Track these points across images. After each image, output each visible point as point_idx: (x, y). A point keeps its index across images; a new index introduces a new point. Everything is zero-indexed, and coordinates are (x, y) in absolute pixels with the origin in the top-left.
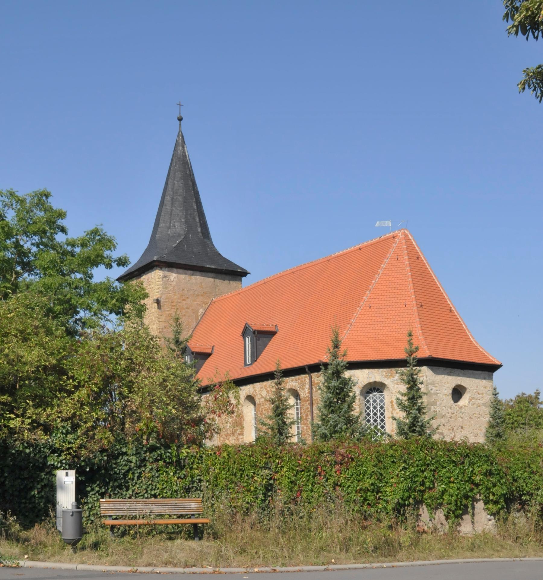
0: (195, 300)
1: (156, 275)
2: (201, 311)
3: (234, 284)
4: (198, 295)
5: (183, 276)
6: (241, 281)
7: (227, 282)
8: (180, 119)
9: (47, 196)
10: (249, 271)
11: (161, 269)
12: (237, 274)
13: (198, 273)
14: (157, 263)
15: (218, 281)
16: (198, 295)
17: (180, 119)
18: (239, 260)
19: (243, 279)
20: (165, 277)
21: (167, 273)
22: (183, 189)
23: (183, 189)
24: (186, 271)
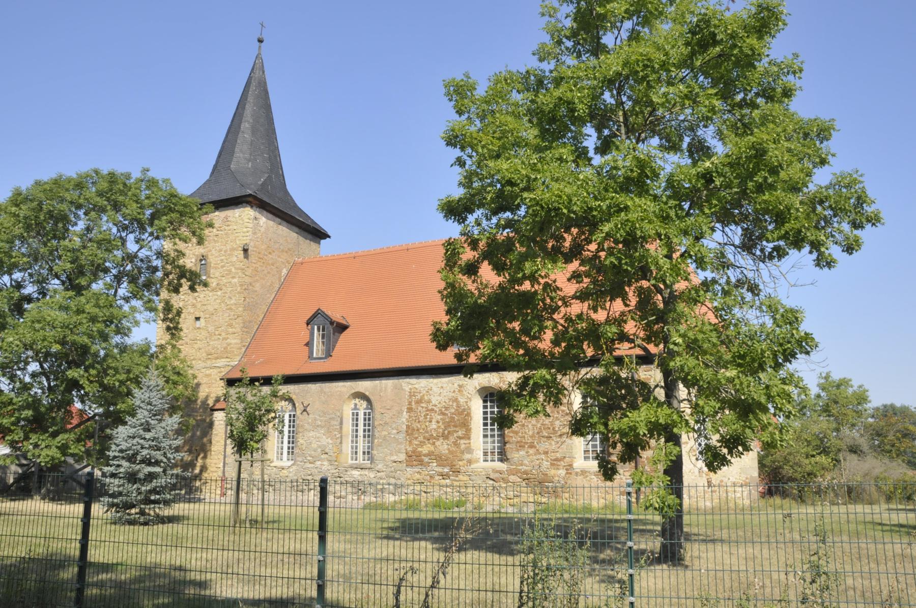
0: (279, 257)
1: (246, 214)
2: (285, 271)
3: (313, 245)
4: (283, 251)
5: (271, 223)
6: (319, 243)
7: (308, 241)
8: (260, 41)
9: (827, 378)
10: (329, 233)
11: (252, 207)
12: (317, 234)
13: (285, 223)
14: (250, 199)
15: (301, 238)
16: (283, 251)
17: (260, 41)
18: (323, 223)
19: (322, 241)
20: (256, 218)
21: (258, 215)
22: (255, 112)
23: (255, 112)
24: (274, 217)
